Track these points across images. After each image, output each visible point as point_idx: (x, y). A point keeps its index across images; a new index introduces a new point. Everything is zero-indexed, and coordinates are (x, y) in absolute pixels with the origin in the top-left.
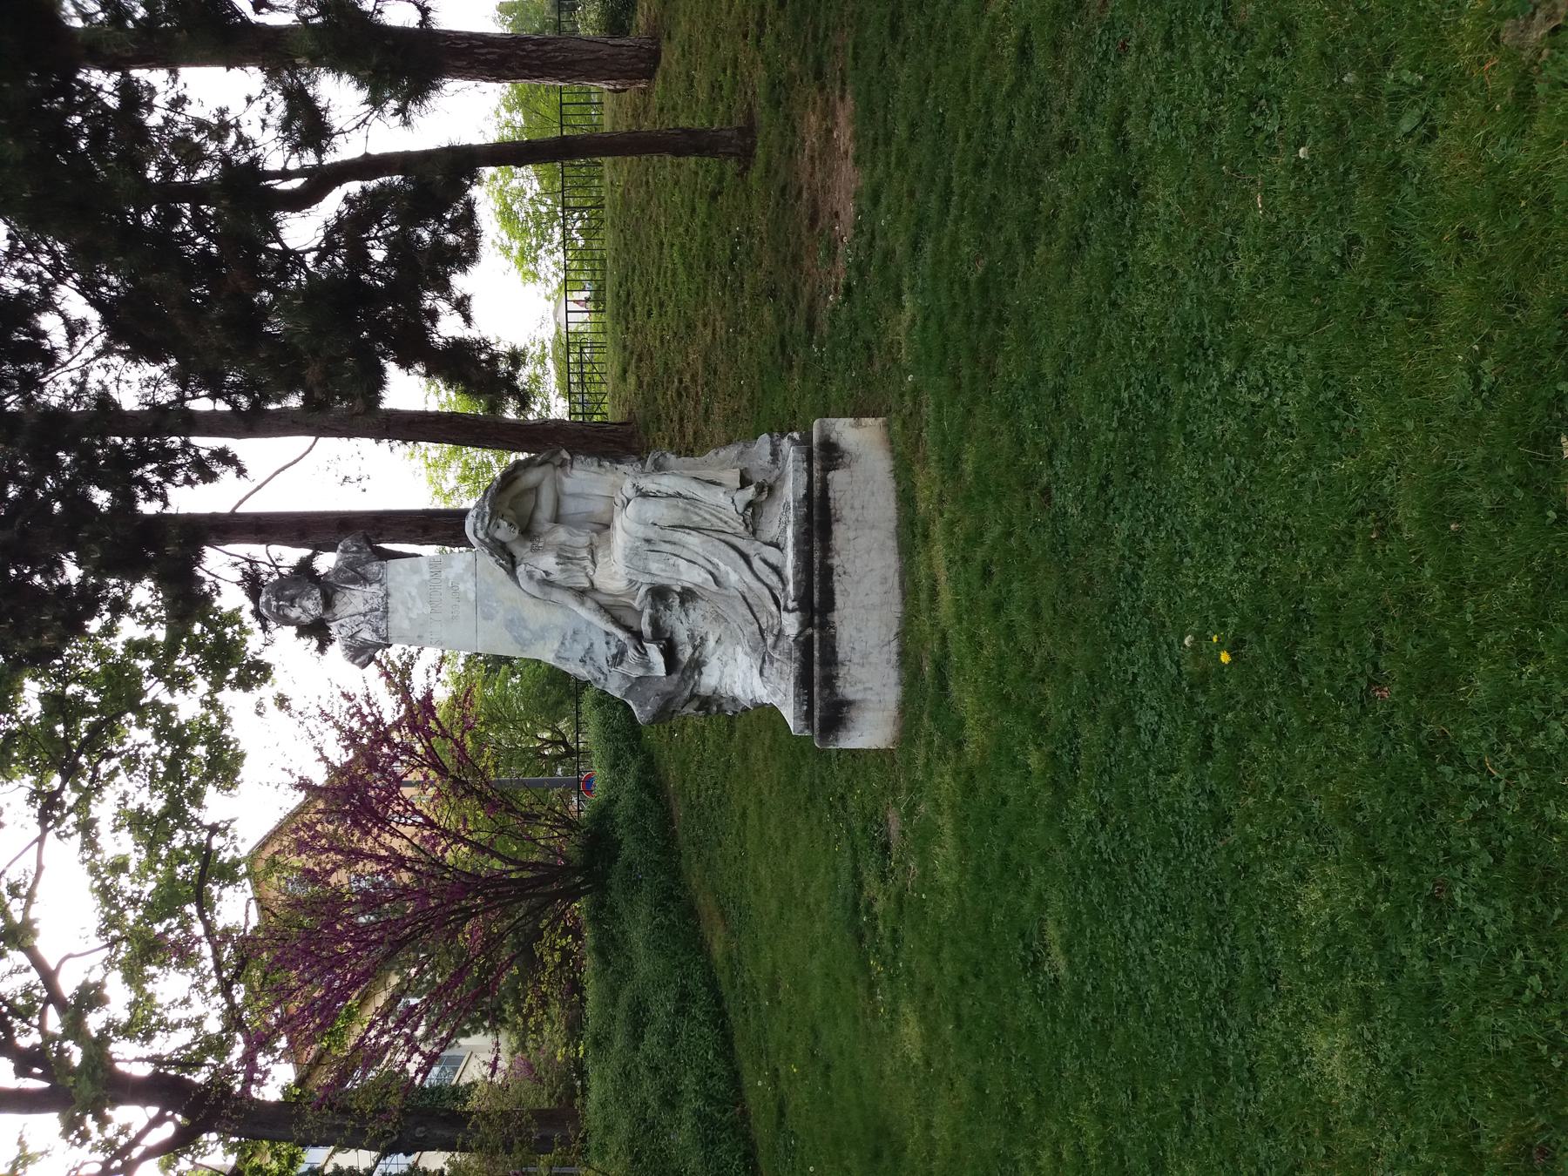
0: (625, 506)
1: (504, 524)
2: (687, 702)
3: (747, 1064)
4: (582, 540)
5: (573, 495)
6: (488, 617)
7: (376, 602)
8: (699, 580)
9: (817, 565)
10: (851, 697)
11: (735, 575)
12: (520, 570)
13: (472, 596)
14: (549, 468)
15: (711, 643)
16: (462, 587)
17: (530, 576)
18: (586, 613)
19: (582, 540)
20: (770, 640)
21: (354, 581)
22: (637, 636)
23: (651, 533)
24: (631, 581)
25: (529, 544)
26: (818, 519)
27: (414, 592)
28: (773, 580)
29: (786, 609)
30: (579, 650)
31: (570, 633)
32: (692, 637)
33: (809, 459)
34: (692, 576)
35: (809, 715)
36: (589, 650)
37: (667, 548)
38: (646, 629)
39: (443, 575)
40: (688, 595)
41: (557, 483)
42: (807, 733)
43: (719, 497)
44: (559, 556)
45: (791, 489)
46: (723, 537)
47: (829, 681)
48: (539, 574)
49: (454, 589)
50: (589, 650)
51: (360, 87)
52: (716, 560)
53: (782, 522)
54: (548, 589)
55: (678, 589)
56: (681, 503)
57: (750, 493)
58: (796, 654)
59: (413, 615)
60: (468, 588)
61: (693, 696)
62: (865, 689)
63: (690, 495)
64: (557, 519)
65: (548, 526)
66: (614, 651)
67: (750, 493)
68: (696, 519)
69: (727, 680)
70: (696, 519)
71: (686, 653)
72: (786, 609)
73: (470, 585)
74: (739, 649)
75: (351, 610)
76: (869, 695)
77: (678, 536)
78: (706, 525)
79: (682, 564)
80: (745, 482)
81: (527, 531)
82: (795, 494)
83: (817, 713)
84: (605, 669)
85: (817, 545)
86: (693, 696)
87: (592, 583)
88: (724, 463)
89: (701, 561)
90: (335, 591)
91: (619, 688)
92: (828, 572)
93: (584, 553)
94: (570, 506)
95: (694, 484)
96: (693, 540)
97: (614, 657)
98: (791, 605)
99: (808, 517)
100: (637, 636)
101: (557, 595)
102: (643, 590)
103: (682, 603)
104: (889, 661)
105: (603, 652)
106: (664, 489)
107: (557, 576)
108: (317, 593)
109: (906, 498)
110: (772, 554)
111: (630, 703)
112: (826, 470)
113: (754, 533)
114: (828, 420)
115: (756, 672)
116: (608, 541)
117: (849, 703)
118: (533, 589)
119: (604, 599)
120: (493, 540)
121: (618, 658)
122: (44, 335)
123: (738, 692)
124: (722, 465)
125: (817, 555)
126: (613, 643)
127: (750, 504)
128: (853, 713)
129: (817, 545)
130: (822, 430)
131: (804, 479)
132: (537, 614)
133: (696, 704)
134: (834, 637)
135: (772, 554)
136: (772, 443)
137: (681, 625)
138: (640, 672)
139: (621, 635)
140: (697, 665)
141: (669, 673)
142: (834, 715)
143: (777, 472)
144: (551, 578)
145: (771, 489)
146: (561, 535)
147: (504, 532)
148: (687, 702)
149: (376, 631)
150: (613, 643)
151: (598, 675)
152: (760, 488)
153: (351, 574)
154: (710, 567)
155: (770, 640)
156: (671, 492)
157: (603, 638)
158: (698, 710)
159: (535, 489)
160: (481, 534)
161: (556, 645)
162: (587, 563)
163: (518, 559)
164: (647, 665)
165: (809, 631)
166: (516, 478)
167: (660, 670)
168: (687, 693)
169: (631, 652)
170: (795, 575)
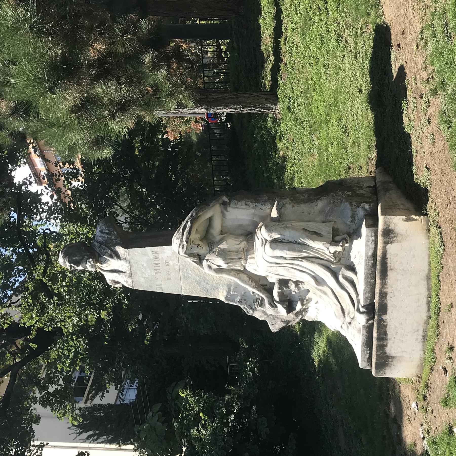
3: (363, 151)
9: (377, 290)
13: (177, 268)
16: (171, 263)
27: (145, 265)
42: (368, 368)
47: (382, 347)
49: (167, 264)
62: (403, 352)
76: (404, 354)
83: (374, 360)
85: (378, 281)
87: (245, 268)
98: (362, 310)
99: (374, 265)
104: (417, 339)
106: (287, 238)
112: (386, 243)
114: (388, 217)
117: (392, 357)
128: (395, 362)
129: (378, 281)
130: (385, 222)
131: (372, 246)
134: (386, 327)
136: (352, 210)
156: (291, 240)
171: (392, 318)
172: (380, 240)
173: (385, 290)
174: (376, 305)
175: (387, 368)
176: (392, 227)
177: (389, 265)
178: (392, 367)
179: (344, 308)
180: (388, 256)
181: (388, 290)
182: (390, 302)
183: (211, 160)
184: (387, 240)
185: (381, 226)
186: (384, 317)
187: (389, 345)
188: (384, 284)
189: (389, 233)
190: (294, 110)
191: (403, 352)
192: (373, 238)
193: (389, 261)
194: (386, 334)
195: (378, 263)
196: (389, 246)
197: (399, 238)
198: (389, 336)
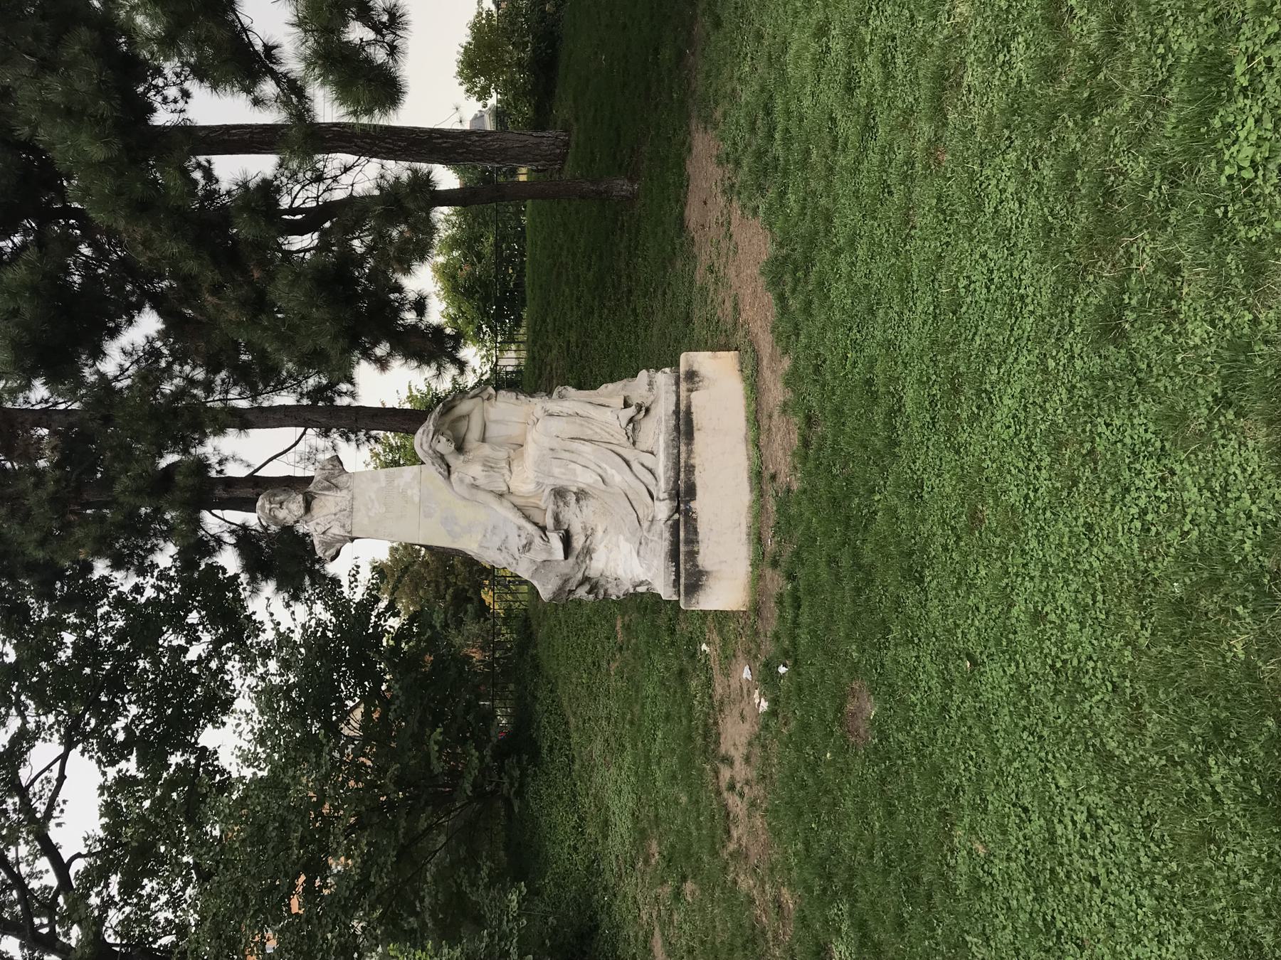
0: (535, 424)
1: (443, 439)
2: (581, 584)
4: (502, 454)
5: (496, 422)
6: (428, 515)
7: (344, 504)
8: (590, 481)
10: (708, 568)
11: (618, 476)
12: (454, 477)
13: (417, 499)
14: (478, 400)
15: (599, 534)
16: (409, 492)
17: (462, 481)
18: (504, 513)
19: (502, 454)
20: (646, 524)
21: (328, 489)
22: (543, 529)
23: (555, 444)
24: (538, 483)
25: (462, 457)
26: (684, 427)
27: (373, 496)
28: (648, 478)
29: (658, 499)
30: (497, 541)
31: (490, 528)
32: (585, 528)
33: (677, 384)
34: (585, 478)
35: (676, 582)
36: (505, 541)
37: (566, 455)
38: (549, 522)
39: (396, 483)
40: (581, 495)
41: (483, 411)
42: (675, 598)
43: (607, 416)
44: (484, 465)
45: (663, 409)
46: (610, 446)
47: (692, 555)
48: (468, 480)
50: (505, 541)
51: (429, 365)
52: (604, 465)
53: (656, 432)
54: (474, 491)
55: (575, 490)
56: (578, 420)
57: (631, 411)
58: (667, 535)
59: (372, 514)
60: (414, 493)
61: (586, 579)
62: (721, 562)
63: (585, 414)
64: (483, 440)
65: (476, 444)
66: (524, 542)
67: (631, 411)
68: (590, 432)
69: (612, 564)
70: (590, 432)
71: (578, 543)
72: (658, 499)
73: (416, 491)
74: (621, 537)
75: (325, 511)
77: (576, 445)
78: (596, 438)
79: (579, 469)
80: (627, 405)
81: (460, 448)
82: (666, 410)
83: (682, 581)
84: (517, 556)
86: (586, 579)
88: (612, 392)
89: (593, 466)
90: (313, 498)
91: (527, 570)
92: (690, 469)
93: (504, 464)
94: (493, 431)
95: (589, 406)
96: (587, 448)
97: (524, 547)
99: (677, 428)
100: (543, 529)
101: (482, 496)
102: (548, 491)
103: (578, 500)
105: (515, 543)
106: (565, 410)
107: (481, 481)
108: (300, 498)
109: (755, 419)
110: (648, 460)
111: (535, 583)
112: (690, 390)
113: (634, 443)
115: (635, 554)
116: (522, 455)
118: (466, 493)
119: (519, 502)
120: (435, 452)
121: (527, 547)
122: (200, 656)
123: (620, 573)
124: (610, 395)
125: (683, 456)
126: (523, 536)
127: (631, 420)
129: (683, 448)
130: (687, 361)
132: (465, 513)
133: (587, 587)
134: (695, 520)
135: (648, 460)
137: (575, 518)
138: (544, 557)
139: (530, 528)
140: (588, 552)
141: (566, 557)
142: (694, 581)
143: (652, 398)
144: (477, 483)
145: (647, 410)
146: (486, 450)
147: (444, 446)
148: (581, 584)
149: (343, 526)
150: (523, 536)
151: (511, 560)
152: (639, 407)
153: (326, 484)
154: (600, 471)
155: (646, 524)
157: (516, 531)
158: (589, 592)
159: (467, 416)
160: (426, 447)
161: (480, 537)
162: (506, 471)
163: (452, 469)
164: (550, 552)
165: (676, 516)
166: (453, 407)
167: (559, 554)
168: (580, 576)
169: (538, 540)
170: (665, 473)
171: (701, 505)
172: (683, 386)
173: (692, 461)
174: (682, 486)
175: (701, 593)
176: (695, 368)
177: (695, 422)
178: (708, 590)
179: (627, 458)
180: (693, 409)
181: (696, 461)
182: (700, 479)
183: (316, 868)
184: (690, 386)
185: (683, 369)
186: (692, 504)
187: (701, 551)
188: (690, 453)
189: (692, 375)
190: (589, 269)
191: (721, 562)
192: (674, 388)
193: (694, 417)
194: (696, 532)
195: (681, 422)
196: (694, 395)
197: (706, 383)
198: (701, 537)
